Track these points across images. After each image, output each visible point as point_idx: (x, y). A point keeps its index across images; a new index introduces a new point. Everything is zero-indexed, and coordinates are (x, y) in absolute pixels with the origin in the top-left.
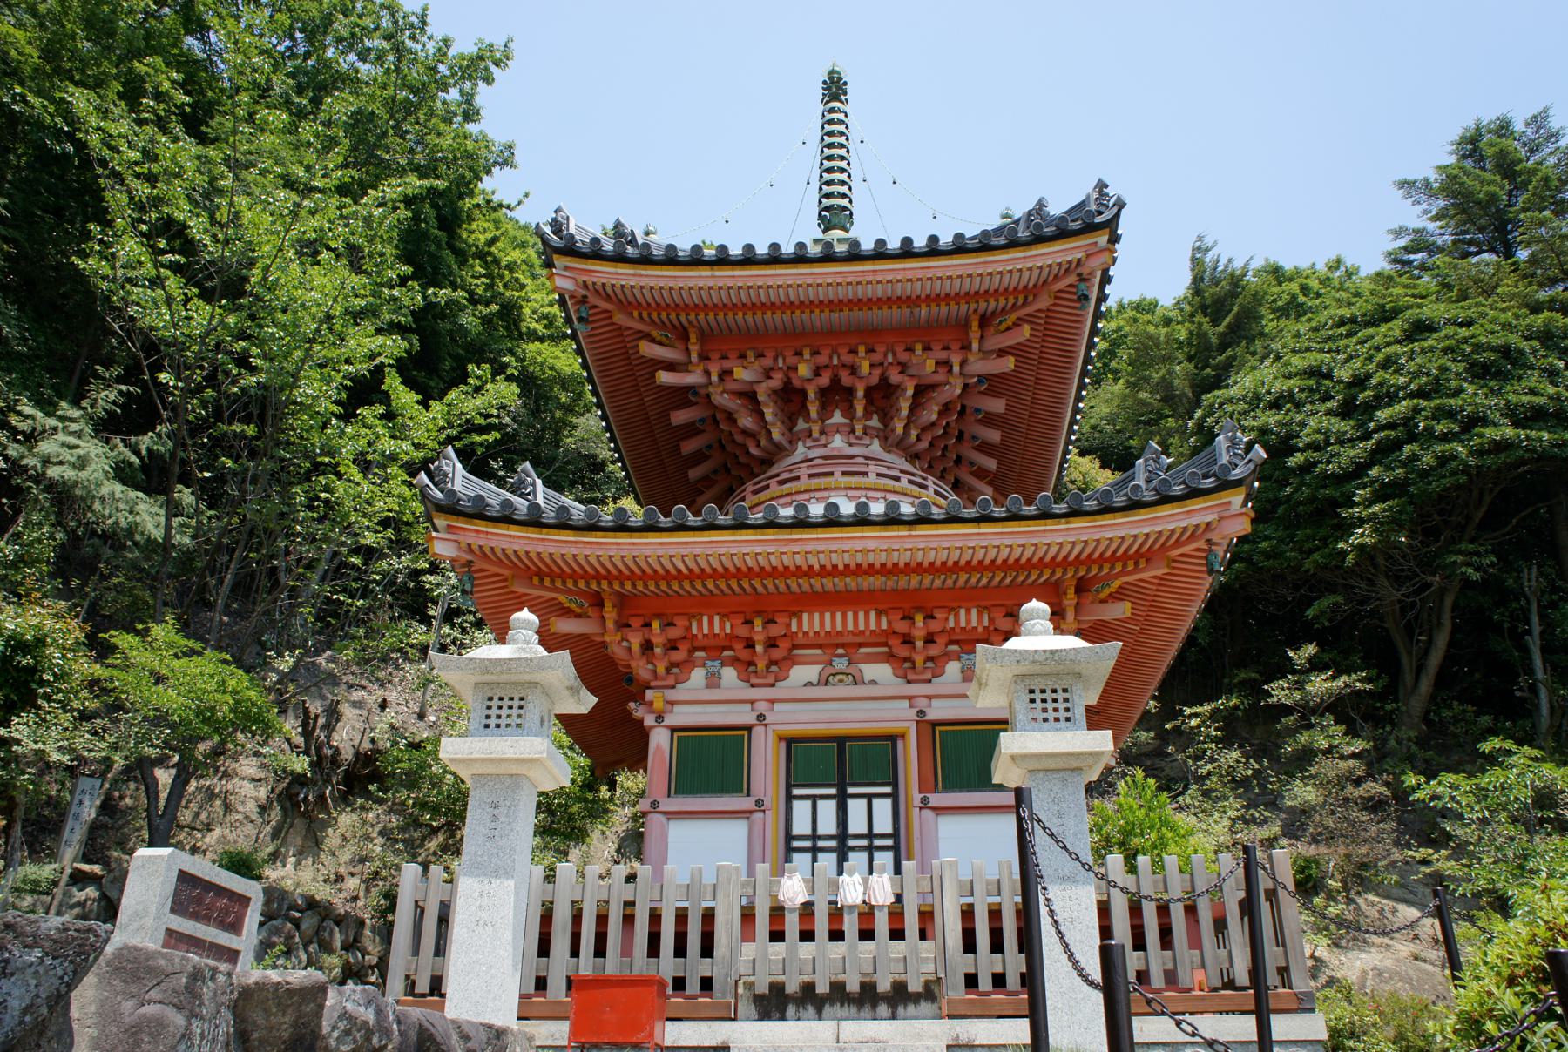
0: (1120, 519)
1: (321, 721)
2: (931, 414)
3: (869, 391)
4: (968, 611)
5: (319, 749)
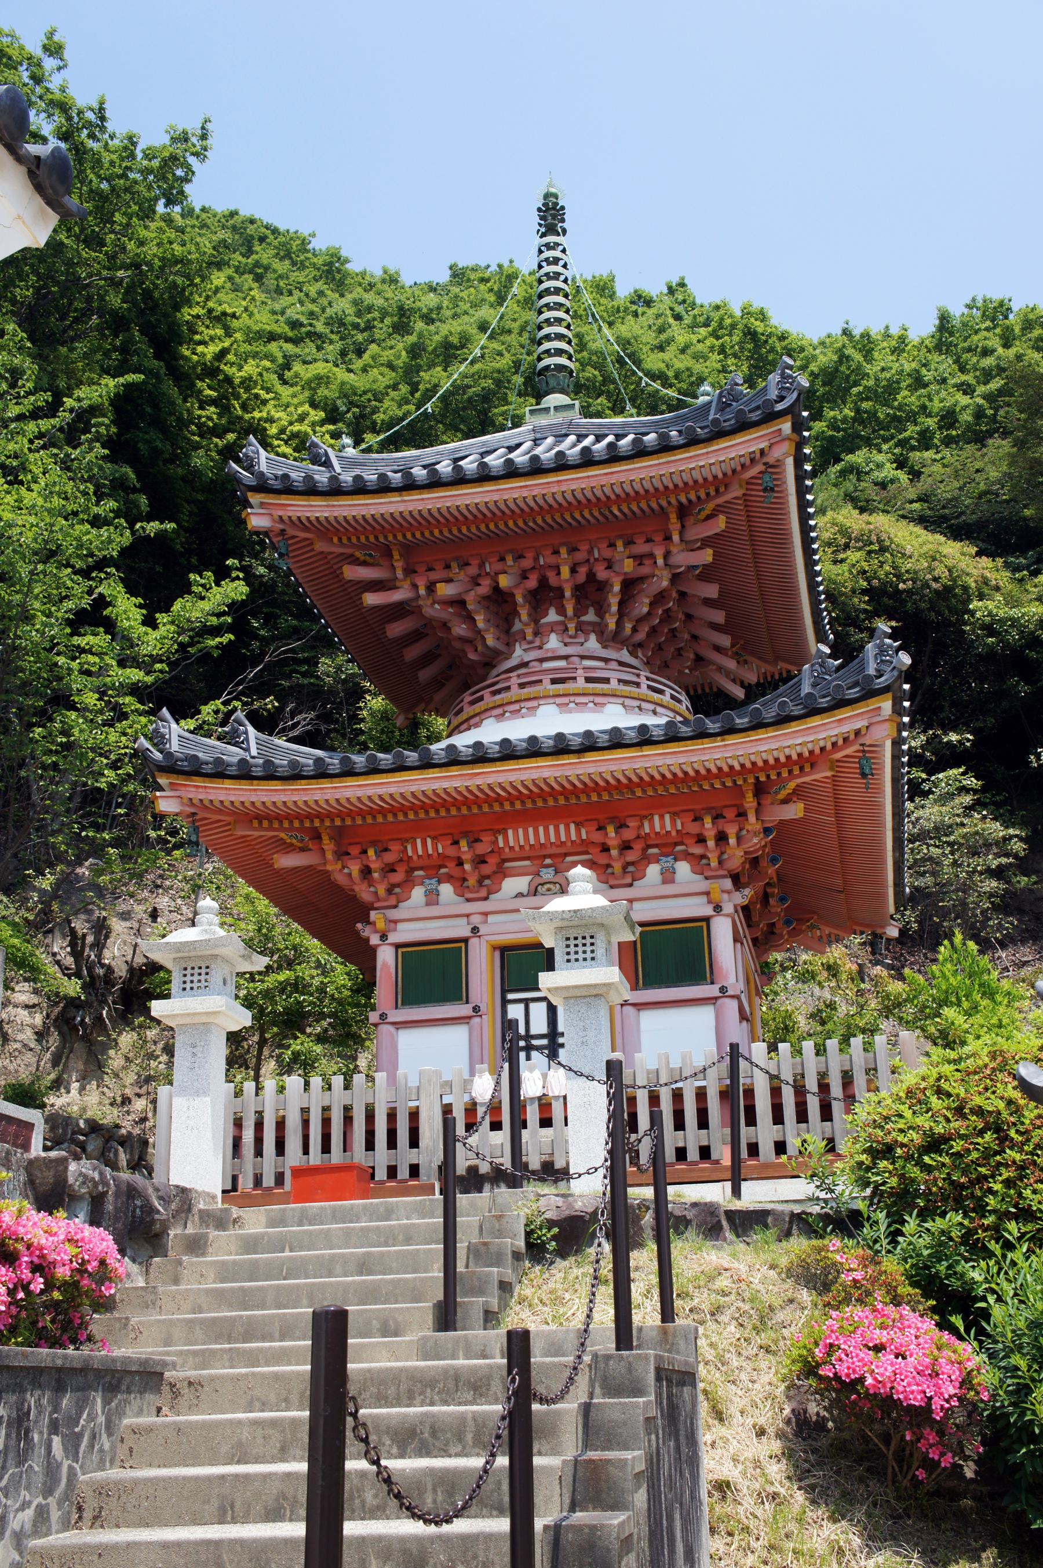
0: (771, 733)
1: (90, 939)
2: (642, 607)
3: (578, 589)
4: (662, 817)
5: (90, 969)
